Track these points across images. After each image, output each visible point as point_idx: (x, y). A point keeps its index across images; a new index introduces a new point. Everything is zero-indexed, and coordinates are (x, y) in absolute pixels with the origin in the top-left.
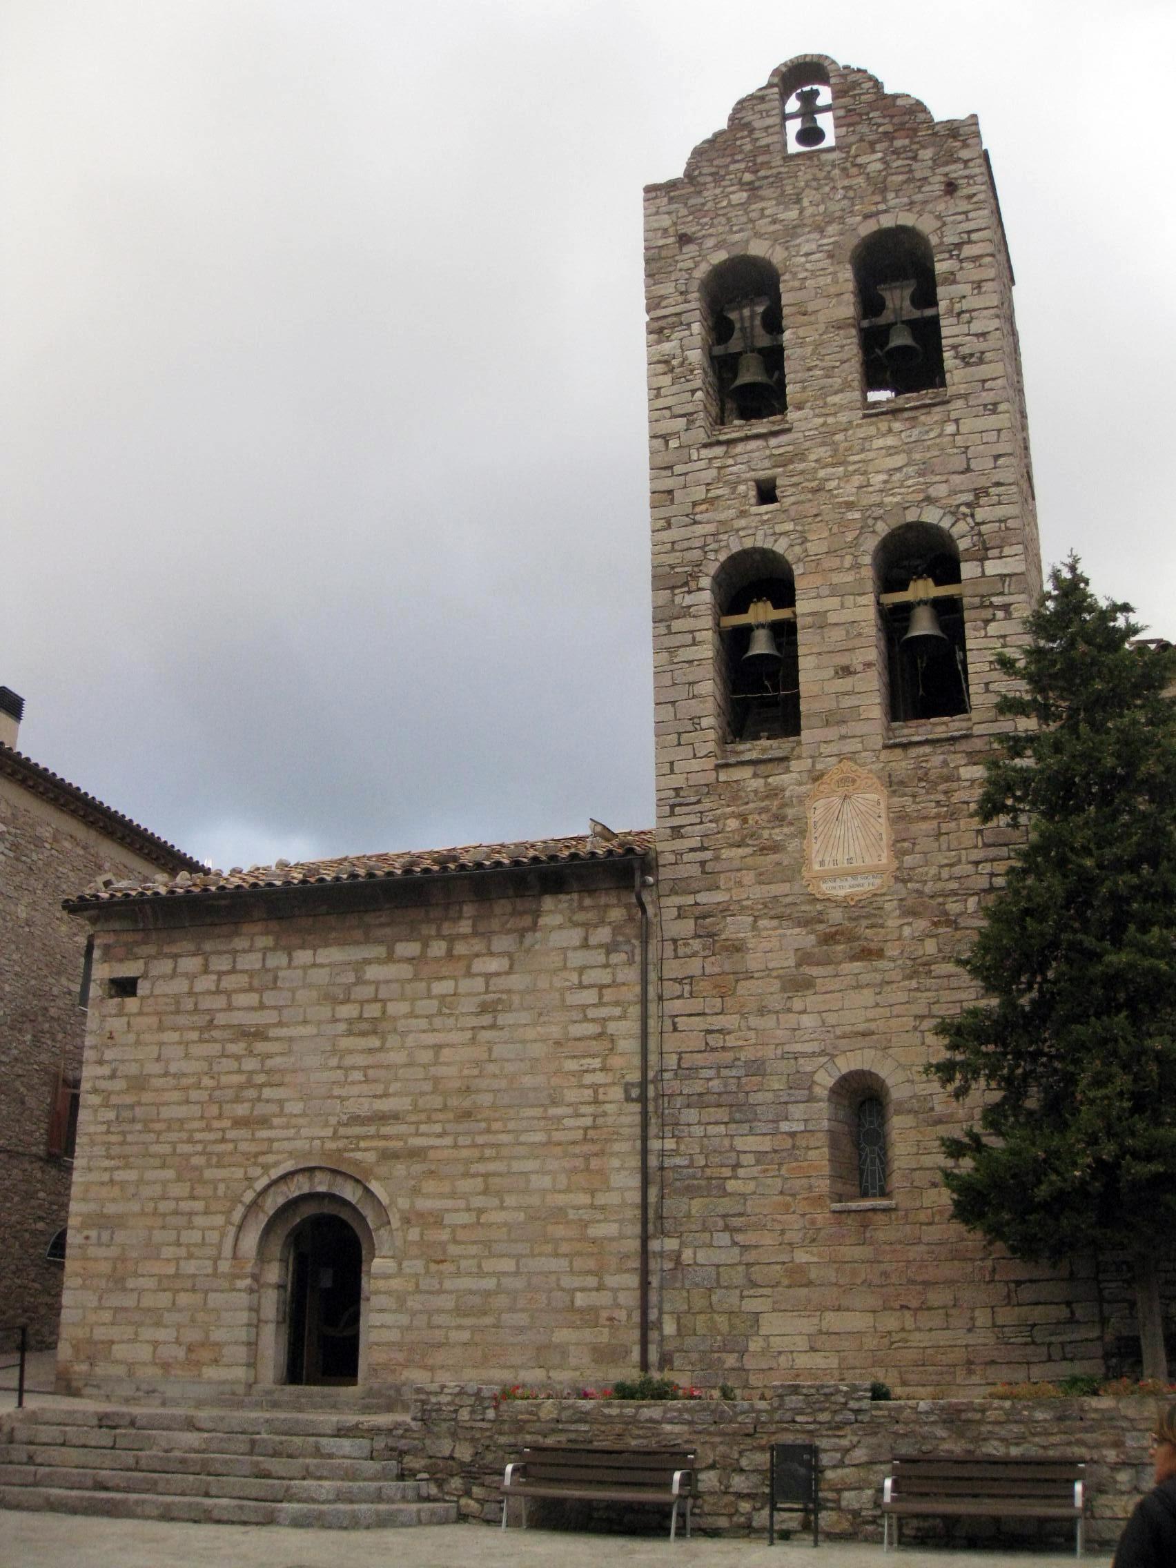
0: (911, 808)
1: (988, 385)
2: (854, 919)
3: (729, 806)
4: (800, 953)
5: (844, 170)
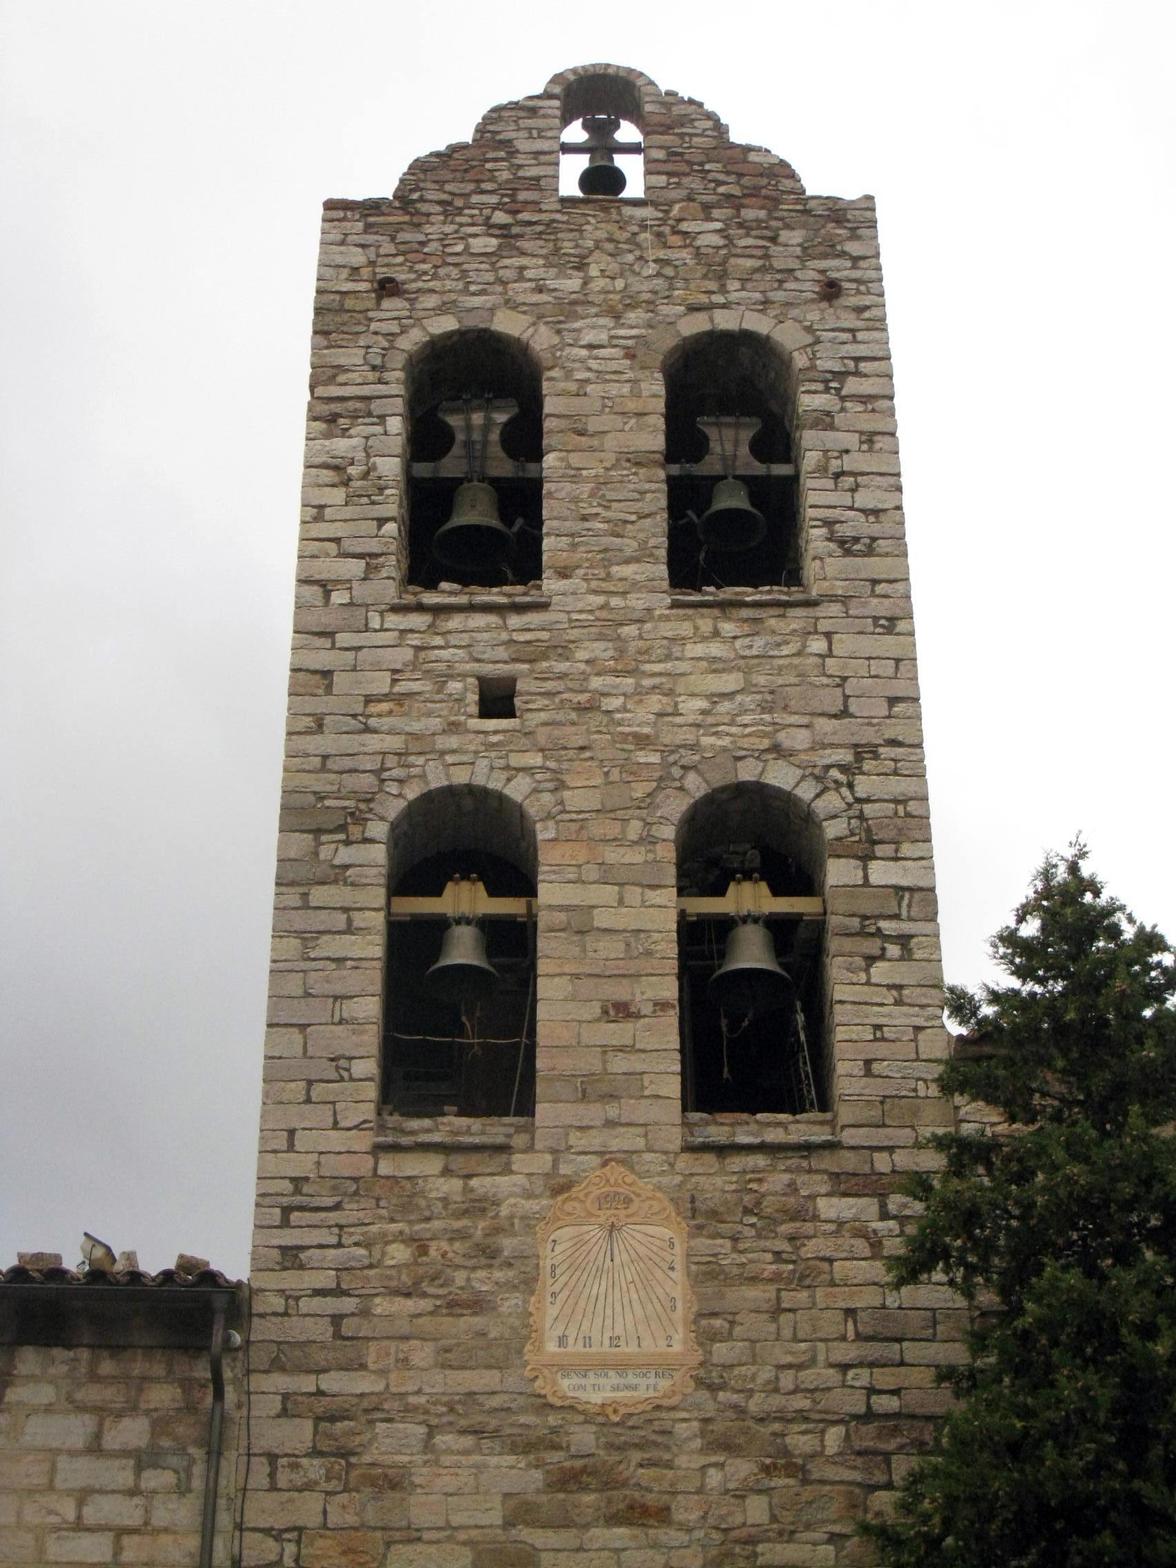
1: (880, 589)
2: (618, 1448)
3: (392, 1220)
4: (512, 1503)
5: (659, 235)
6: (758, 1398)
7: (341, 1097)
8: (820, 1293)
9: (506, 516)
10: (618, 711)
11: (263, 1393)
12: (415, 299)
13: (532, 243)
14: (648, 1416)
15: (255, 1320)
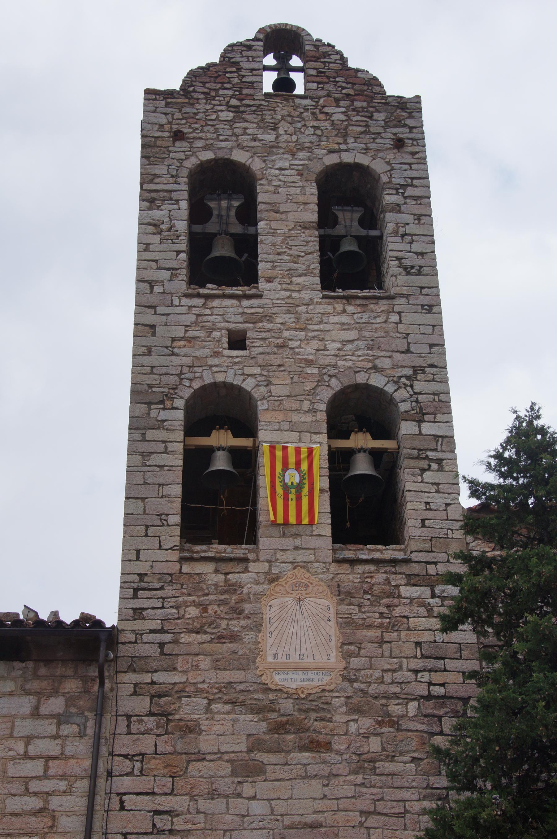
0: (358, 617)
1: (424, 291)
2: (304, 711)
3: (189, 595)
4: (251, 739)
5: (313, 114)
6: (374, 686)
7: (163, 534)
8: (403, 634)
9: (239, 252)
10: (297, 348)
11: (124, 683)
12: (192, 142)
13: (251, 116)
14: (319, 695)
15: (120, 645)
